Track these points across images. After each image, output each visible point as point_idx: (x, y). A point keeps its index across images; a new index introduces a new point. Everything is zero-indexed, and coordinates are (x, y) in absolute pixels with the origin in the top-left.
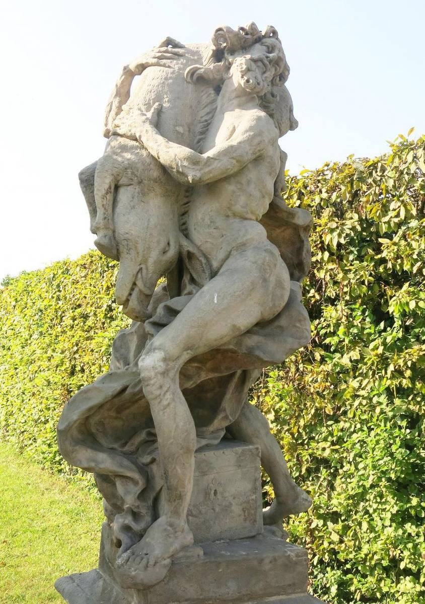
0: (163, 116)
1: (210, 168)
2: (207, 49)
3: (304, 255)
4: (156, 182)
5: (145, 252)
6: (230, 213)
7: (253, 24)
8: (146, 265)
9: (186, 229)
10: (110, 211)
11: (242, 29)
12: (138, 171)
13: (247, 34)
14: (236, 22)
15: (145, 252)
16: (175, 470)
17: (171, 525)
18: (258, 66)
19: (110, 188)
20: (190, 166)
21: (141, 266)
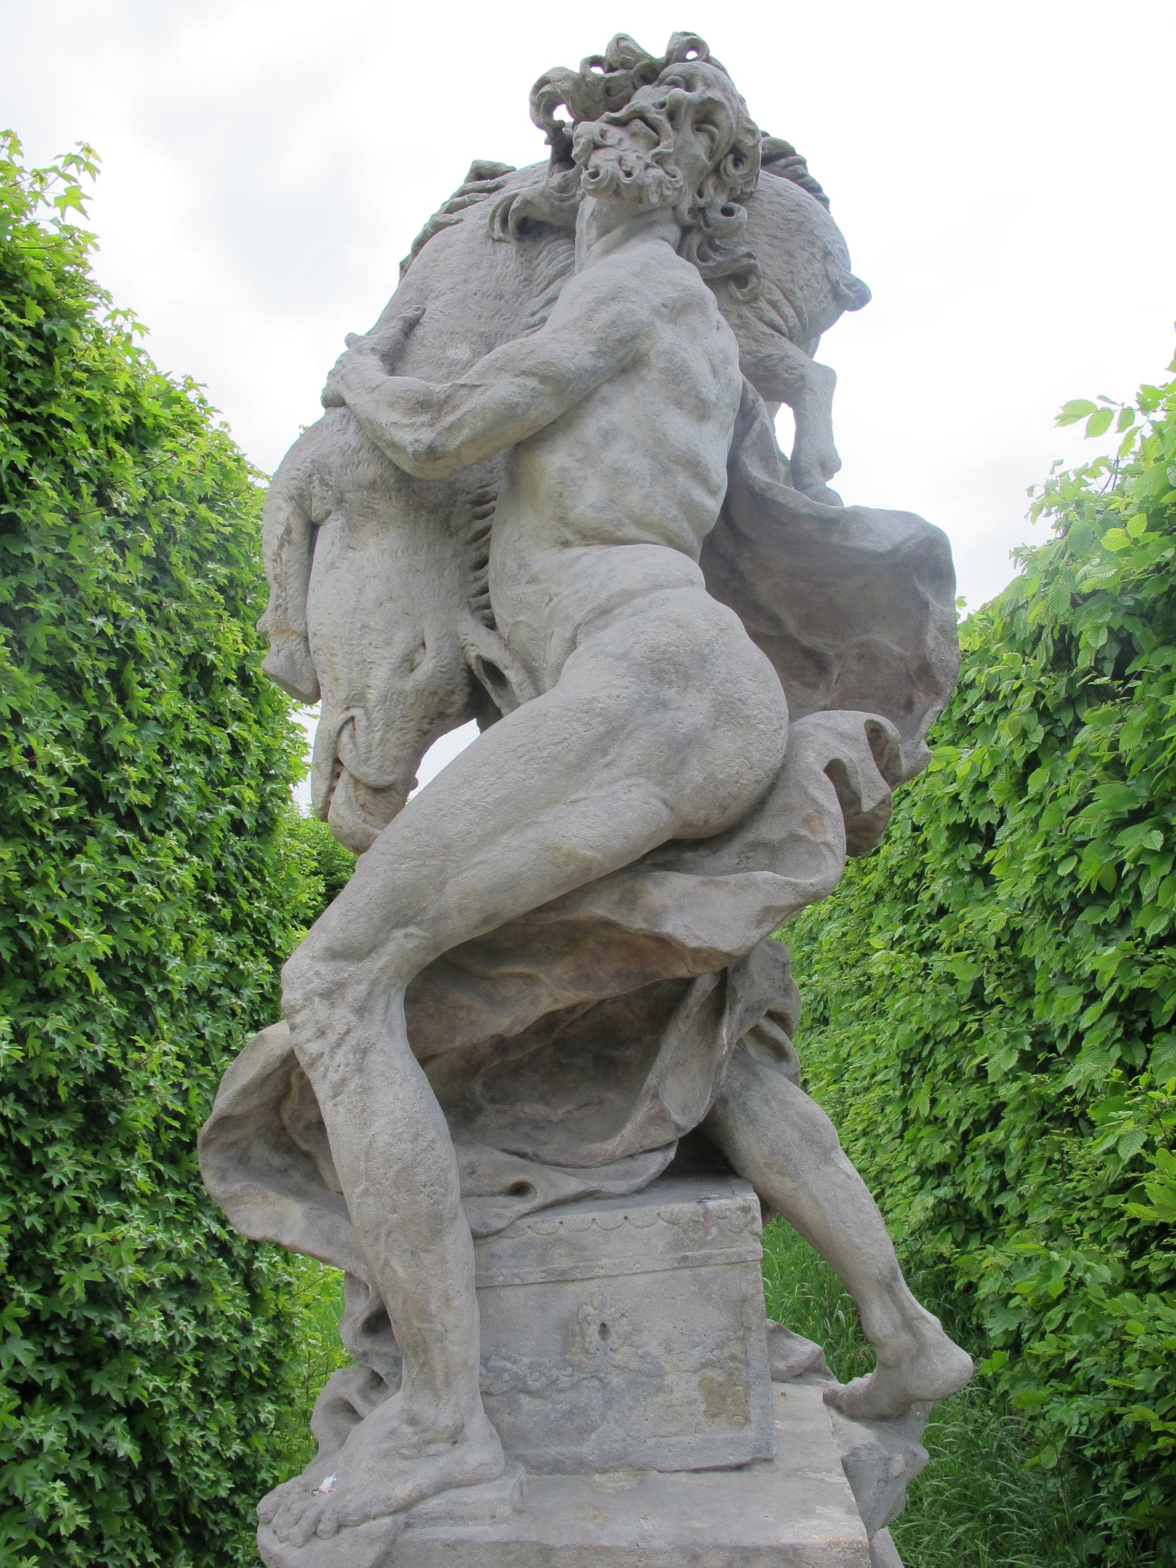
0: (419, 331)
1: (459, 413)
3: (930, 643)
4: (375, 491)
5: (354, 675)
6: (568, 534)
7: (1143, 387)
8: (364, 708)
9: (488, 606)
11: (595, 61)
12: (330, 473)
14: (574, 49)
15: (354, 675)
16: (388, 1269)
17: (412, 1421)
18: (634, 135)
19: (288, 531)
20: (406, 421)
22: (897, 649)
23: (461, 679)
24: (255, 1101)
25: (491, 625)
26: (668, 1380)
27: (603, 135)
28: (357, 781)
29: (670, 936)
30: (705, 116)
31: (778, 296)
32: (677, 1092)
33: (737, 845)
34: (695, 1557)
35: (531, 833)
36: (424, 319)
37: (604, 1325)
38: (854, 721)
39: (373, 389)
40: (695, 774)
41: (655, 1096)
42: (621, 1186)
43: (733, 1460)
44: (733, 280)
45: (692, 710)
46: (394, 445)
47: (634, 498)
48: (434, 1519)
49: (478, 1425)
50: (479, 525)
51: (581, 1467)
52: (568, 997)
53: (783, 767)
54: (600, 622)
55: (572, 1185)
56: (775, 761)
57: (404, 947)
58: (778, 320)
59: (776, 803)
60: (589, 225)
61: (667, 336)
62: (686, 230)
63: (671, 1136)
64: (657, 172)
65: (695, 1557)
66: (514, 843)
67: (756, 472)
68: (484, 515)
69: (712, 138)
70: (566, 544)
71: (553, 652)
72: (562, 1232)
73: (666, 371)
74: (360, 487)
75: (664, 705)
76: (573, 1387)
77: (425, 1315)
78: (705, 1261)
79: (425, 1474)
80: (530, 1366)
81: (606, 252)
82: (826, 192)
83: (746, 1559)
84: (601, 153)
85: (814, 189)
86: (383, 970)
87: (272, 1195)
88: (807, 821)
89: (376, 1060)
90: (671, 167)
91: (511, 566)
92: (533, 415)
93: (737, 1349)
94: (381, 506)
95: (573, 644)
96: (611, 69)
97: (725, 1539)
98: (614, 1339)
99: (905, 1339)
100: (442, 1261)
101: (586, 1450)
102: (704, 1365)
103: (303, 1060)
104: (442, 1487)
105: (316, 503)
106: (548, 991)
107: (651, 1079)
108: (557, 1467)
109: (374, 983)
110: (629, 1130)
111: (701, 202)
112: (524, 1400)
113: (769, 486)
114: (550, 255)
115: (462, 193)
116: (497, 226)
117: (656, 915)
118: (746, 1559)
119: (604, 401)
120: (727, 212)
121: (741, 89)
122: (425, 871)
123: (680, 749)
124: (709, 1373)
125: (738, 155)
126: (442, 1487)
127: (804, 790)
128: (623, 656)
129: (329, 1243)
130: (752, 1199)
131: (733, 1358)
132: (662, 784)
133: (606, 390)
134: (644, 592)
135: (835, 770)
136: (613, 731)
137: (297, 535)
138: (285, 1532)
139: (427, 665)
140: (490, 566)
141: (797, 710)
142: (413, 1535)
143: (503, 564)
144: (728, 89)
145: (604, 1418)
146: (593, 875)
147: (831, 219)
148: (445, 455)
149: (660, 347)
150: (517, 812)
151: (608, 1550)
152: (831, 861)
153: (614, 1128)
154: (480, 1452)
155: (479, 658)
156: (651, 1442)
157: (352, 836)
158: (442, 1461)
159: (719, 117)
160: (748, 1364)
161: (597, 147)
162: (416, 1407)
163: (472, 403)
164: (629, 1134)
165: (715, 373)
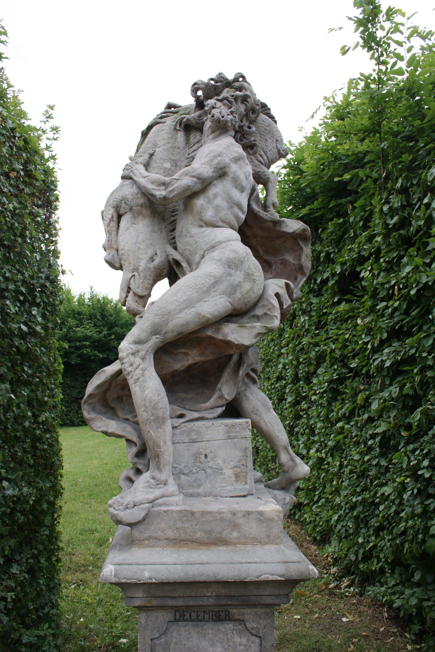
0: (154, 157)
2: (191, 101)
3: (303, 260)
6: (202, 224)
9: (175, 243)
10: (114, 233)
11: (212, 79)
13: (217, 82)
14: (206, 75)
17: (154, 478)
19: (112, 217)
21: (134, 273)
22: (292, 261)
23: (167, 264)
24: (101, 390)
25: (175, 248)
26: (224, 471)
27: (215, 104)
28: (135, 294)
29: (230, 341)
30: (245, 99)
31: (262, 153)
32: (226, 391)
33: (248, 316)
34: (235, 514)
35: (193, 309)
36: (155, 154)
37: (206, 455)
38: (282, 282)
39: (145, 177)
40: (238, 295)
41: (220, 390)
42: (210, 416)
43: (242, 494)
44: (249, 147)
45: (238, 277)
46: (152, 195)
47: (222, 214)
48: (160, 505)
49: (171, 480)
50: (173, 219)
51: (199, 495)
52: (198, 359)
53: (262, 294)
54: (212, 250)
55: (196, 415)
56: (260, 292)
57: (155, 341)
58: (262, 160)
59: (261, 304)
60: (208, 129)
61: (234, 167)
62: (236, 132)
63: (224, 402)
64: (231, 117)
65: (235, 514)
66: (188, 312)
67: (255, 207)
68: (174, 216)
69: (246, 105)
70: (201, 226)
71: (197, 258)
72: (194, 427)
73: (233, 178)
74: (138, 205)
75: (231, 275)
76: (197, 472)
77: (159, 447)
78: (235, 437)
79: (157, 493)
80: (185, 467)
81: (214, 138)
82: (276, 119)
83: (249, 514)
84: (215, 110)
85: (272, 118)
86: (149, 347)
87: (104, 418)
88: (269, 310)
89: (147, 373)
90: (235, 115)
91: (185, 232)
92: (194, 189)
93: (244, 462)
94: (144, 212)
95: (203, 257)
96: (217, 82)
97: (243, 509)
98: (209, 459)
99: (291, 463)
100: (164, 431)
101: (200, 491)
102: (235, 467)
103: (125, 373)
104: (162, 497)
105: (122, 209)
106: (192, 357)
107: (219, 385)
108: (192, 495)
109: (147, 351)
110: (212, 400)
111: (242, 124)
112: (182, 476)
113: (259, 212)
114: (194, 137)
115: (165, 113)
116: (178, 126)
117: (224, 335)
118: (249, 514)
119: (214, 185)
120: (249, 128)
121: (255, 91)
122: (163, 319)
123: (234, 288)
124: (236, 469)
125: (254, 111)
126: (162, 497)
127: (269, 301)
128: (220, 260)
129: (124, 431)
130: (249, 420)
131: (243, 465)
132: (229, 297)
133: (215, 182)
134: (225, 242)
135: (277, 295)
136: (217, 282)
137: (115, 219)
138: (118, 508)
139: (158, 260)
140: (177, 230)
141: (266, 279)
142: (156, 509)
143: (182, 231)
144: (251, 92)
145: (205, 482)
146: (209, 323)
147: (277, 128)
148: (169, 199)
149: (232, 171)
150: (189, 303)
151: (210, 512)
152: (276, 321)
153: (208, 399)
154: (172, 487)
155: (173, 259)
156: (219, 489)
157: (133, 310)
158: (162, 489)
159: (249, 100)
160: (247, 467)
161: (214, 108)
162: (154, 474)
163: (177, 184)
164: (212, 402)
165: (246, 178)
